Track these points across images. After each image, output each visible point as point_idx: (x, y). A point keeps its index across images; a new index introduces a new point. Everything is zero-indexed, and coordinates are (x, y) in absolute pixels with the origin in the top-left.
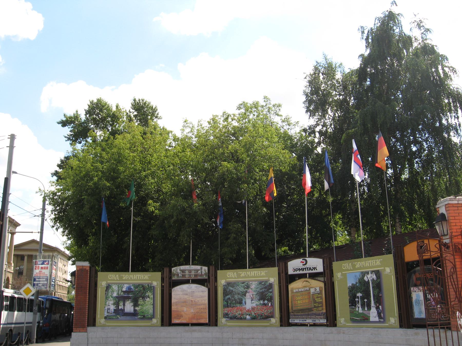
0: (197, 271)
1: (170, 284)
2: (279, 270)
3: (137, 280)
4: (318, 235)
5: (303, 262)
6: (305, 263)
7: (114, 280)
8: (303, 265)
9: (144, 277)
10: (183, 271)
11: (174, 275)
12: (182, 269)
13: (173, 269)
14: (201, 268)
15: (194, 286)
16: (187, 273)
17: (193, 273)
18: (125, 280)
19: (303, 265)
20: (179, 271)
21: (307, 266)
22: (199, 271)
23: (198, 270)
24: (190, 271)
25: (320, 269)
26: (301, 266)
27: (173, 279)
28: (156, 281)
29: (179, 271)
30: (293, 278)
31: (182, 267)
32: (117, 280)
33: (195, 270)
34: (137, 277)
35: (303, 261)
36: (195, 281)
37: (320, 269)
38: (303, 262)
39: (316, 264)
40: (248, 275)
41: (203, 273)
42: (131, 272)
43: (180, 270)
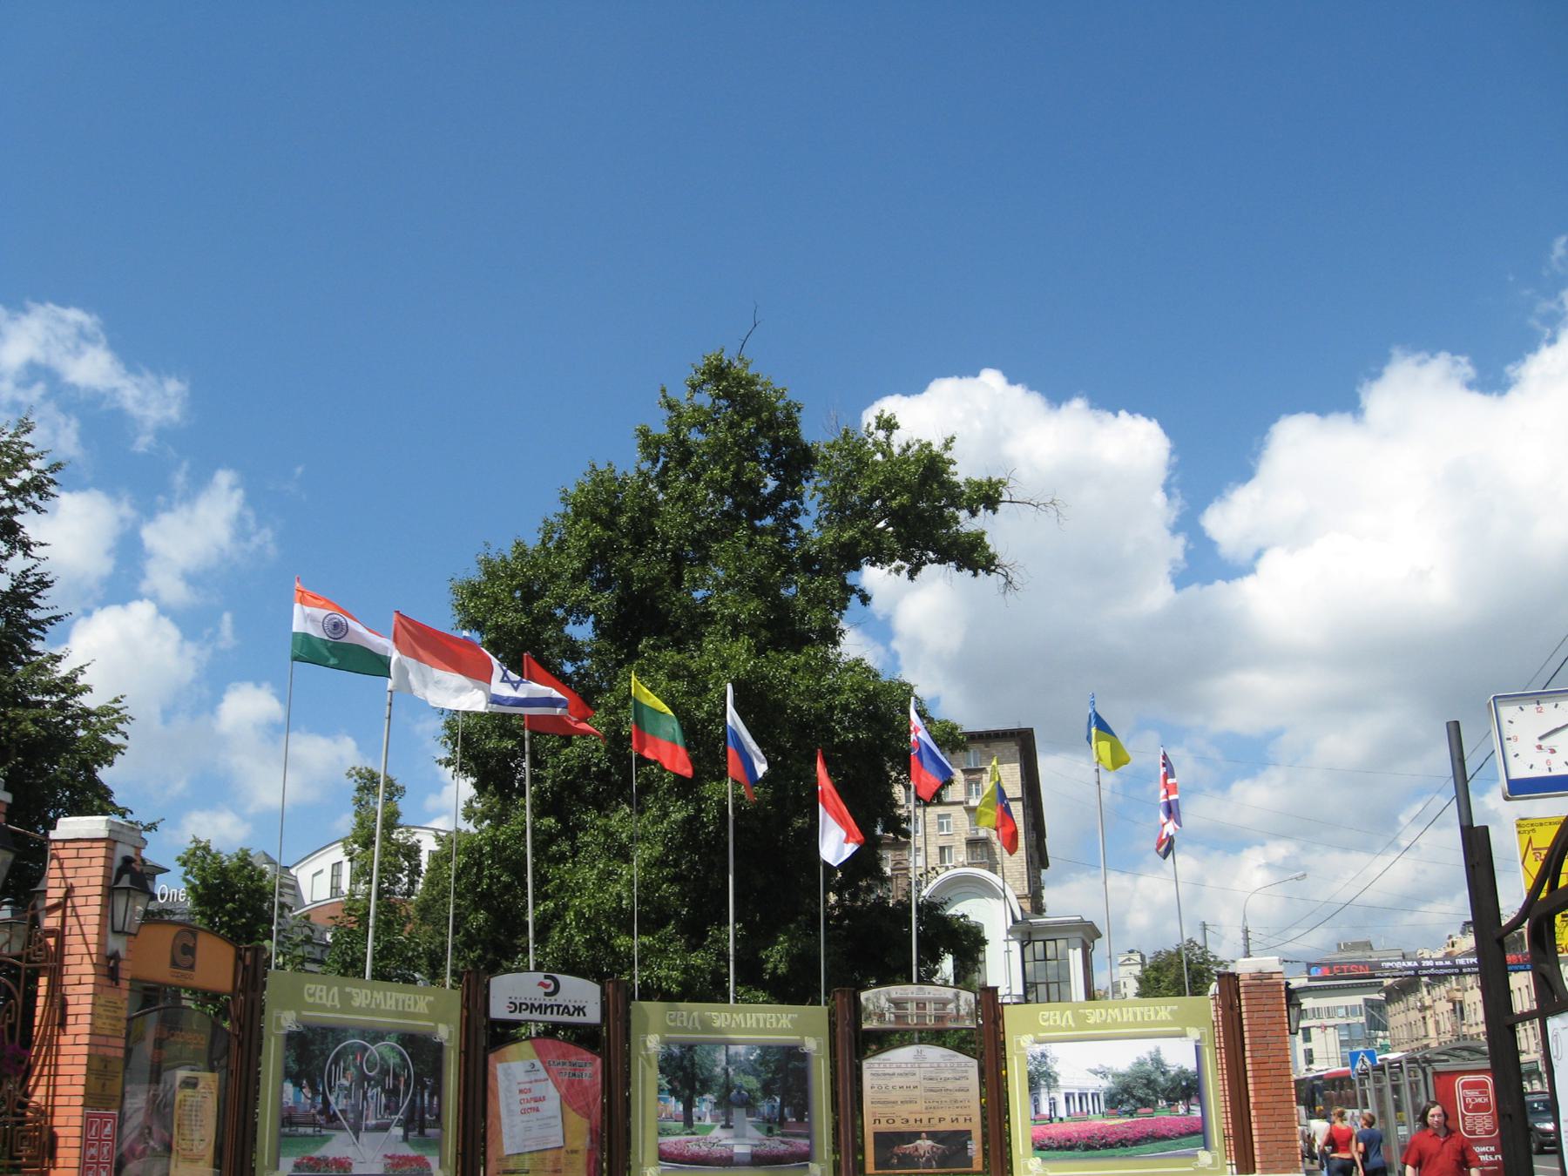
0: (945, 1003)
1: (858, 1043)
2: (831, 1014)
3: (758, 1031)
4: (568, 668)
5: (547, 986)
6: (551, 989)
7: (1060, 1028)
8: (547, 994)
9: (1157, 1013)
10: (898, 1004)
11: (869, 1017)
12: (894, 995)
13: (863, 995)
14: (957, 996)
15: (934, 1053)
16: (911, 1008)
17: (931, 1009)
18: (1096, 1026)
19: (547, 994)
20: (884, 1003)
21: (559, 999)
22: (951, 1006)
23: (950, 1001)
24: (921, 1005)
25: (593, 1016)
26: (537, 995)
27: (865, 1026)
28: (814, 1035)
29: (884, 1003)
30: (882, 1040)
31: (896, 991)
32: (1069, 1028)
33: (936, 1001)
34: (1135, 1015)
35: (548, 981)
36: (937, 1037)
37: (593, 1016)
38: (547, 986)
39: (583, 997)
40: (1115, 1021)
41: (962, 1012)
42: (736, 1001)
43: (890, 1000)
